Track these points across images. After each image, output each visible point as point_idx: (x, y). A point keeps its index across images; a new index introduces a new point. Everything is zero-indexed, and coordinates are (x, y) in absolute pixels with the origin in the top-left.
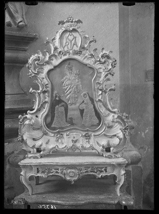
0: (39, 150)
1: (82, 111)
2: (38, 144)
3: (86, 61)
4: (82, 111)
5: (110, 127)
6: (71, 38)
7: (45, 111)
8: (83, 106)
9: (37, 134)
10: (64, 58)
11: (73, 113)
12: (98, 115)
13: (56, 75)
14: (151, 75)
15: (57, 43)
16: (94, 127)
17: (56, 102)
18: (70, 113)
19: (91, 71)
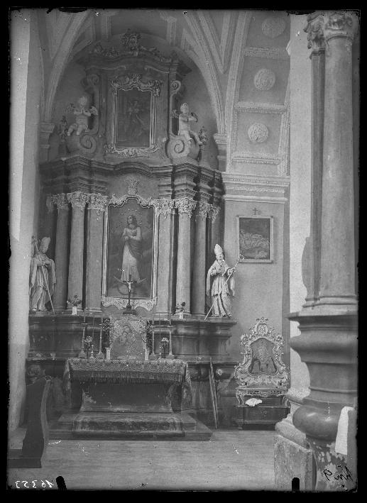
0: (246, 384)
1: (267, 365)
2: (246, 380)
3: (269, 340)
4: (267, 365)
5: (281, 373)
6: (262, 327)
7: (249, 363)
8: (268, 362)
9: (244, 375)
10: (259, 337)
11: (263, 366)
12: (275, 367)
13: (255, 347)
14: (143, 447)
15: (255, 330)
16: (274, 373)
17: (255, 360)
18: (262, 366)
19: (272, 345)
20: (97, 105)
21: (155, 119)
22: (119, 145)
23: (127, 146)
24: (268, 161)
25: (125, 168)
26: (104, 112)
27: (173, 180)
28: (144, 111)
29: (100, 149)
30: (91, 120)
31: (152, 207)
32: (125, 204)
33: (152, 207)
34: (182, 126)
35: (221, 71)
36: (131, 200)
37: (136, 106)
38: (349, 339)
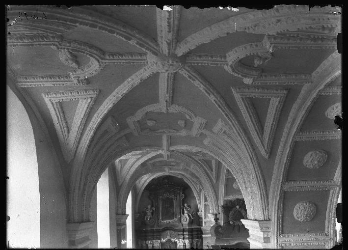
20: (154, 206)
21: (175, 210)
22: (163, 219)
23: (166, 219)
24: (282, 160)
25: (167, 228)
26: (157, 208)
27: (183, 233)
28: (172, 206)
29: (156, 222)
30: (152, 213)
31: (176, 242)
32: (166, 242)
33: (176, 242)
34: (186, 212)
35: (199, 191)
36: (169, 240)
37: (169, 203)
38: (145, 248)
